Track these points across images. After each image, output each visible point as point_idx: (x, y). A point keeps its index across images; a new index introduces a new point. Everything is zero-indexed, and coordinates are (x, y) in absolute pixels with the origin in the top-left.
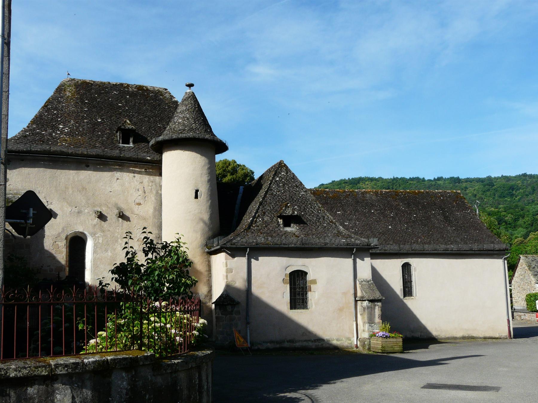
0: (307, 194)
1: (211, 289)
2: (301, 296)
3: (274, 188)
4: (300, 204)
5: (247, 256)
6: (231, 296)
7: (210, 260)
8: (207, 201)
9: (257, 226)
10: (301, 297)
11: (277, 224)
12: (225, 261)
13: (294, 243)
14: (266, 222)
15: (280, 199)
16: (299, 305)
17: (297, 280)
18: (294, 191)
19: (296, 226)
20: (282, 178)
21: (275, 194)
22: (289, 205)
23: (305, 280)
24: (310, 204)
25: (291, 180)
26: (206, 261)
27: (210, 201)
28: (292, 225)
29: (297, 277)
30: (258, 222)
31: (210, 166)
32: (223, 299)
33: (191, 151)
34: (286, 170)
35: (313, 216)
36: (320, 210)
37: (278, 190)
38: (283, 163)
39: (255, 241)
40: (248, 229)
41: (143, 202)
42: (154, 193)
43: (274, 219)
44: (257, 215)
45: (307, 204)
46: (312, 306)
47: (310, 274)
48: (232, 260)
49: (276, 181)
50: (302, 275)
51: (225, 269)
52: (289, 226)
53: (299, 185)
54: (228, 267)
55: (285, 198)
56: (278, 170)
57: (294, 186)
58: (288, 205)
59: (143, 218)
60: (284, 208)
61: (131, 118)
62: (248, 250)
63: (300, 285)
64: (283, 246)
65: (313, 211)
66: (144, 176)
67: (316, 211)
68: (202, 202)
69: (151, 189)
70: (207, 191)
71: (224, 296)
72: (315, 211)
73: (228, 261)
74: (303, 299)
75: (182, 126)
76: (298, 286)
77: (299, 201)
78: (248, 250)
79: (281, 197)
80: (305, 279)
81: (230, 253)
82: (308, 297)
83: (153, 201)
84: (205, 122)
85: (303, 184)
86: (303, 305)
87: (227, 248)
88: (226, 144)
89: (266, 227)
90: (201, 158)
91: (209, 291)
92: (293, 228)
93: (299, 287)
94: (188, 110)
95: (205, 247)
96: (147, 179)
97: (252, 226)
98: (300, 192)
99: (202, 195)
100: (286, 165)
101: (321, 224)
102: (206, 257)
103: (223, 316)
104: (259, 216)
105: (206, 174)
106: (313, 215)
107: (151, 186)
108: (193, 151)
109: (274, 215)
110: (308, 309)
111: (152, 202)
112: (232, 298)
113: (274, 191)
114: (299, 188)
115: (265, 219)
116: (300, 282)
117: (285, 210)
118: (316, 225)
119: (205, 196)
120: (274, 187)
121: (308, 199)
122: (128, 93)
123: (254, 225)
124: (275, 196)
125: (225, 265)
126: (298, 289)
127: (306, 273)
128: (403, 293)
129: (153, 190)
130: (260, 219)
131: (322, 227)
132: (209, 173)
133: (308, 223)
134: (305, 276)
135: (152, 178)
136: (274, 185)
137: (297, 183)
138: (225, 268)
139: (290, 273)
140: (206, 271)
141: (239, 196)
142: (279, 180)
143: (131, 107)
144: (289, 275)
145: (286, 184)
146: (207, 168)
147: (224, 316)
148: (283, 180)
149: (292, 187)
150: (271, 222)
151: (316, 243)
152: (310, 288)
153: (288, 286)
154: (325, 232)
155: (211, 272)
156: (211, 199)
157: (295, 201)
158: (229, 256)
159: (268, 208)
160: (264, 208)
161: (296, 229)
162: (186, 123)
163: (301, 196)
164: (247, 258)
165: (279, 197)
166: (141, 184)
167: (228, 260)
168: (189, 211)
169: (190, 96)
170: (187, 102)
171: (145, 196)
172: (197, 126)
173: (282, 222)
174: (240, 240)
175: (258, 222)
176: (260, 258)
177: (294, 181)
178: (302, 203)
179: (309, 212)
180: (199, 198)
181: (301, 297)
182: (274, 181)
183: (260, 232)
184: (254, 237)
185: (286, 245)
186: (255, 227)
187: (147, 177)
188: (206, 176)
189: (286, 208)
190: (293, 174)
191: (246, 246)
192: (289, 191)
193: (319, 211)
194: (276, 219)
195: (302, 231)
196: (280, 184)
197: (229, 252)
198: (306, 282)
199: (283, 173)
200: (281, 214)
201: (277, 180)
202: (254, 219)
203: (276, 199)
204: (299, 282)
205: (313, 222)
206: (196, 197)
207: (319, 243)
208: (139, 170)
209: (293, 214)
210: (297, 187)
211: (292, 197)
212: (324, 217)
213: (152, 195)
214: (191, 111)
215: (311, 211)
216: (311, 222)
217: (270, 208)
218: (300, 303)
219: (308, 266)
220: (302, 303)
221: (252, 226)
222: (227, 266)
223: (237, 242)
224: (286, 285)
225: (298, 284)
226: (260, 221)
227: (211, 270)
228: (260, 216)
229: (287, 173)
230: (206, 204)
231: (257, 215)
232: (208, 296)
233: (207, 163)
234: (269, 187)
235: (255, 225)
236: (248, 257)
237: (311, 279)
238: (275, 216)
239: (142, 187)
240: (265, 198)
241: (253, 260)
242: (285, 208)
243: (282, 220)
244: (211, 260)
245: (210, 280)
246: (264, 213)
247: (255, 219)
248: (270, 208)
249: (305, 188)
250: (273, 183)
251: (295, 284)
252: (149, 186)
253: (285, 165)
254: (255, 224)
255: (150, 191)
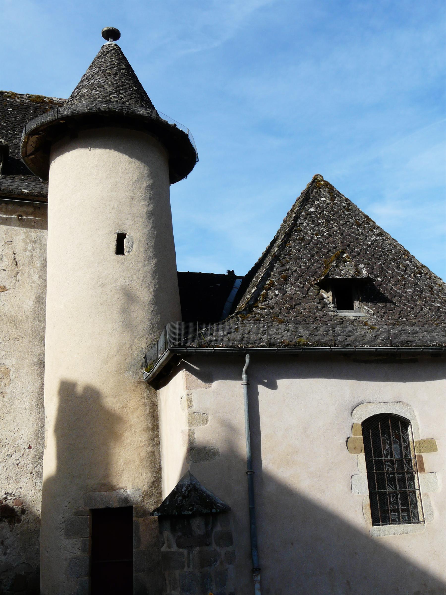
0: (384, 240)
1: (161, 478)
2: (397, 485)
3: (306, 227)
4: (369, 259)
5: (244, 376)
6: (203, 488)
7: (157, 402)
8: (145, 260)
9: (269, 307)
10: (398, 487)
11: (320, 303)
12: (184, 393)
13: (368, 342)
14: (291, 298)
15: (321, 249)
16: (394, 511)
17: (385, 444)
18: (353, 233)
19: (366, 306)
20: (323, 209)
21: (309, 238)
22: (347, 256)
23: (404, 441)
24: (394, 260)
25: (343, 212)
26: (145, 404)
27: (154, 261)
28: (356, 304)
29: (383, 433)
30: (270, 297)
31: (152, 182)
32: (180, 498)
33: (105, 147)
34: (329, 193)
35: (404, 285)
36: (421, 273)
37: (315, 230)
38: (322, 180)
39: (264, 337)
40: (247, 314)
41: (12, 284)
42: (39, 265)
43: (312, 291)
44: (268, 282)
45: (386, 260)
46: (431, 513)
47: (417, 424)
48: (204, 389)
49: (309, 214)
50: (395, 427)
51: (187, 414)
52: (351, 307)
53: (364, 221)
54: (196, 407)
55: (335, 248)
56: (312, 193)
57: (353, 224)
58: (344, 256)
59: (10, 320)
60: (334, 264)
61: (9, 138)
62: (247, 360)
63: (392, 456)
64: (339, 348)
65: (403, 275)
66: (15, 228)
67: (410, 275)
68: (133, 261)
69: (32, 257)
70: (144, 239)
71: (184, 489)
72: (407, 274)
73: (193, 391)
74: (405, 495)
75: (88, 99)
76: (387, 457)
77: (366, 253)
78: (247, 360)
79: (325, 246)
80: (406, 439)
81: (197, 368)
82: (417, 487)
83: (34, 282)
84: (142, 96)
85: (372, 221)
86: (407, 510)
87: (188, 356)
88: (190, 137)
89: (292, 308)
90: (130, 163)
91: (154, 482)
92: (360, 311)
93: (391, 461)
94: (104, 71)
95: (142, 369)
96: (23, 236)
97: (257, 307)
98: (367, 236)
99: (134, 246)
100: (328, 183)
101: (426, 302)
102: (145, 395)
103: (181, 550)
104: (272, 284)
105: (144, 200)
106: (406, 283)
107: (30, 251)
108: (110, 148)
109: (310, 283)
110: (419, 522)
111: (33, 284)
112: (208, 496)
113: (306, 234)
114: (365, 227)
115: (290, 291)
116: (391, 448)
117: (336, 266)
118: (416, 305)
119: (142, 250)
120: (305, 224)
121: (388, 251)
122: (12, 105)
123: (260, 305)
124: (309, 244)
125: (185, 404)
126: (389, 466)
127: (406, 423)
128: (370, 498)
129: (35, 259)
130: (277, 292)
131: (430, 309)
132: (150, 198)
133: (396, 300)
134: (403, 433)
135: (36, 235)
136: (304, 221)
137: (357, 218)
138: (186, 410)
139: (362, 423)
140: (147, 430)
141: (233, 291)
142: (316, 211)
143: (14, 124)
144: (360, 428)
145: (332, 220)
146: (144, 185)
147: (185, 551)
148: (325, 212)
149: (347, 225)
150: (304, 297)
151: (426, 342)
152: (422, 463)
153: (362, 458)
154: (440, 319)
155: (158, 432)
156: (156, 255)
157: (359, 254)
158: (196, 378)
159: (294, 269)
160: (284, 268)
161: (368, 313)
162: (97, 92)
163: (369, 243)
164: (244, 381)
165: (319, 246)
166: (6, 246)
167: (193, 388)
168: (100, 283)
169: (111, 51)
170: (103, 60)
171: (15, 272)
172: (122, 98)
173: (331, 299)
174: (226, 336)
175: (272, 298)
176: (281, 383)
177: (350, 214)
178: (375, 258)
179: (393, 277)
180: (126, 254)
181: (398, 489)
182: (303, 213)
183: (278, 319)
184: (262, 329)
185: (348, 345)
186: (265, 309)
187: (22, 231)
188: (143, 203)
189: (339, 262)
190: (347, 200)
191: (241, 348)
192: (342, 234)
193: (418, 275)
194: (316, 292)
195: (382, 317)
196: (319, 219)
197: (195, 367)
198: (408, 447)
199: (323, 199)
200: (327, 276)
201: (312, 212)
202: (262, 291)
203: (313, 248)
204: (388, 447)
205: (406, 298)
206: (120, 250)
207: (432, 341)
208: (5, 216)
209: (358, 276)
210: (359, 225)
211: (349, 245)
212: (432, 288)
213: (32, 270)
214: (109, 73)
215: (398, 274)
216: (403, 298)
217: (300, 267)
218: (397, 504)
219: (408, 403)
220: (402, 504)
221: (257, 307)
222: (190, 405)
223: (216, 340)
224: (355, 455)
225: (387, 454)
226: (277, 295)
227: (158, 427)
228: (276, 284)
229: (333, 199)
230: (144, 266)
231: (268, 282)
232: (150, 496)
233: (146, 175)
234: (295, 224)
235: (265, 305)
236: (248, 380)
237: (420, 439)
238: (312, 286)
239: (11, 252)
240: (285, 247)
241: (261, 388)
242: (337, 263)
243: (330, 294)
244: (159, 402)
245: (156, 453)
246: (286, 279)
247: (264, 291)
248: (300, 267)
249: (378, 227)
250: (301, 218)
251: (379, 454)
252: (25, 250)
253: (327, 184)
254: (264, 302)
255: (29, 261)
